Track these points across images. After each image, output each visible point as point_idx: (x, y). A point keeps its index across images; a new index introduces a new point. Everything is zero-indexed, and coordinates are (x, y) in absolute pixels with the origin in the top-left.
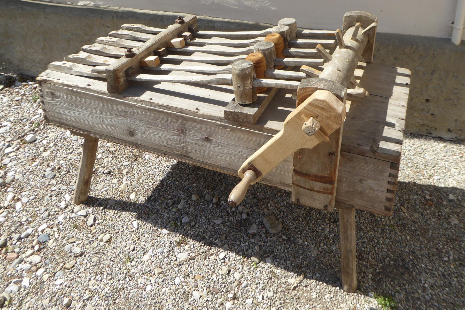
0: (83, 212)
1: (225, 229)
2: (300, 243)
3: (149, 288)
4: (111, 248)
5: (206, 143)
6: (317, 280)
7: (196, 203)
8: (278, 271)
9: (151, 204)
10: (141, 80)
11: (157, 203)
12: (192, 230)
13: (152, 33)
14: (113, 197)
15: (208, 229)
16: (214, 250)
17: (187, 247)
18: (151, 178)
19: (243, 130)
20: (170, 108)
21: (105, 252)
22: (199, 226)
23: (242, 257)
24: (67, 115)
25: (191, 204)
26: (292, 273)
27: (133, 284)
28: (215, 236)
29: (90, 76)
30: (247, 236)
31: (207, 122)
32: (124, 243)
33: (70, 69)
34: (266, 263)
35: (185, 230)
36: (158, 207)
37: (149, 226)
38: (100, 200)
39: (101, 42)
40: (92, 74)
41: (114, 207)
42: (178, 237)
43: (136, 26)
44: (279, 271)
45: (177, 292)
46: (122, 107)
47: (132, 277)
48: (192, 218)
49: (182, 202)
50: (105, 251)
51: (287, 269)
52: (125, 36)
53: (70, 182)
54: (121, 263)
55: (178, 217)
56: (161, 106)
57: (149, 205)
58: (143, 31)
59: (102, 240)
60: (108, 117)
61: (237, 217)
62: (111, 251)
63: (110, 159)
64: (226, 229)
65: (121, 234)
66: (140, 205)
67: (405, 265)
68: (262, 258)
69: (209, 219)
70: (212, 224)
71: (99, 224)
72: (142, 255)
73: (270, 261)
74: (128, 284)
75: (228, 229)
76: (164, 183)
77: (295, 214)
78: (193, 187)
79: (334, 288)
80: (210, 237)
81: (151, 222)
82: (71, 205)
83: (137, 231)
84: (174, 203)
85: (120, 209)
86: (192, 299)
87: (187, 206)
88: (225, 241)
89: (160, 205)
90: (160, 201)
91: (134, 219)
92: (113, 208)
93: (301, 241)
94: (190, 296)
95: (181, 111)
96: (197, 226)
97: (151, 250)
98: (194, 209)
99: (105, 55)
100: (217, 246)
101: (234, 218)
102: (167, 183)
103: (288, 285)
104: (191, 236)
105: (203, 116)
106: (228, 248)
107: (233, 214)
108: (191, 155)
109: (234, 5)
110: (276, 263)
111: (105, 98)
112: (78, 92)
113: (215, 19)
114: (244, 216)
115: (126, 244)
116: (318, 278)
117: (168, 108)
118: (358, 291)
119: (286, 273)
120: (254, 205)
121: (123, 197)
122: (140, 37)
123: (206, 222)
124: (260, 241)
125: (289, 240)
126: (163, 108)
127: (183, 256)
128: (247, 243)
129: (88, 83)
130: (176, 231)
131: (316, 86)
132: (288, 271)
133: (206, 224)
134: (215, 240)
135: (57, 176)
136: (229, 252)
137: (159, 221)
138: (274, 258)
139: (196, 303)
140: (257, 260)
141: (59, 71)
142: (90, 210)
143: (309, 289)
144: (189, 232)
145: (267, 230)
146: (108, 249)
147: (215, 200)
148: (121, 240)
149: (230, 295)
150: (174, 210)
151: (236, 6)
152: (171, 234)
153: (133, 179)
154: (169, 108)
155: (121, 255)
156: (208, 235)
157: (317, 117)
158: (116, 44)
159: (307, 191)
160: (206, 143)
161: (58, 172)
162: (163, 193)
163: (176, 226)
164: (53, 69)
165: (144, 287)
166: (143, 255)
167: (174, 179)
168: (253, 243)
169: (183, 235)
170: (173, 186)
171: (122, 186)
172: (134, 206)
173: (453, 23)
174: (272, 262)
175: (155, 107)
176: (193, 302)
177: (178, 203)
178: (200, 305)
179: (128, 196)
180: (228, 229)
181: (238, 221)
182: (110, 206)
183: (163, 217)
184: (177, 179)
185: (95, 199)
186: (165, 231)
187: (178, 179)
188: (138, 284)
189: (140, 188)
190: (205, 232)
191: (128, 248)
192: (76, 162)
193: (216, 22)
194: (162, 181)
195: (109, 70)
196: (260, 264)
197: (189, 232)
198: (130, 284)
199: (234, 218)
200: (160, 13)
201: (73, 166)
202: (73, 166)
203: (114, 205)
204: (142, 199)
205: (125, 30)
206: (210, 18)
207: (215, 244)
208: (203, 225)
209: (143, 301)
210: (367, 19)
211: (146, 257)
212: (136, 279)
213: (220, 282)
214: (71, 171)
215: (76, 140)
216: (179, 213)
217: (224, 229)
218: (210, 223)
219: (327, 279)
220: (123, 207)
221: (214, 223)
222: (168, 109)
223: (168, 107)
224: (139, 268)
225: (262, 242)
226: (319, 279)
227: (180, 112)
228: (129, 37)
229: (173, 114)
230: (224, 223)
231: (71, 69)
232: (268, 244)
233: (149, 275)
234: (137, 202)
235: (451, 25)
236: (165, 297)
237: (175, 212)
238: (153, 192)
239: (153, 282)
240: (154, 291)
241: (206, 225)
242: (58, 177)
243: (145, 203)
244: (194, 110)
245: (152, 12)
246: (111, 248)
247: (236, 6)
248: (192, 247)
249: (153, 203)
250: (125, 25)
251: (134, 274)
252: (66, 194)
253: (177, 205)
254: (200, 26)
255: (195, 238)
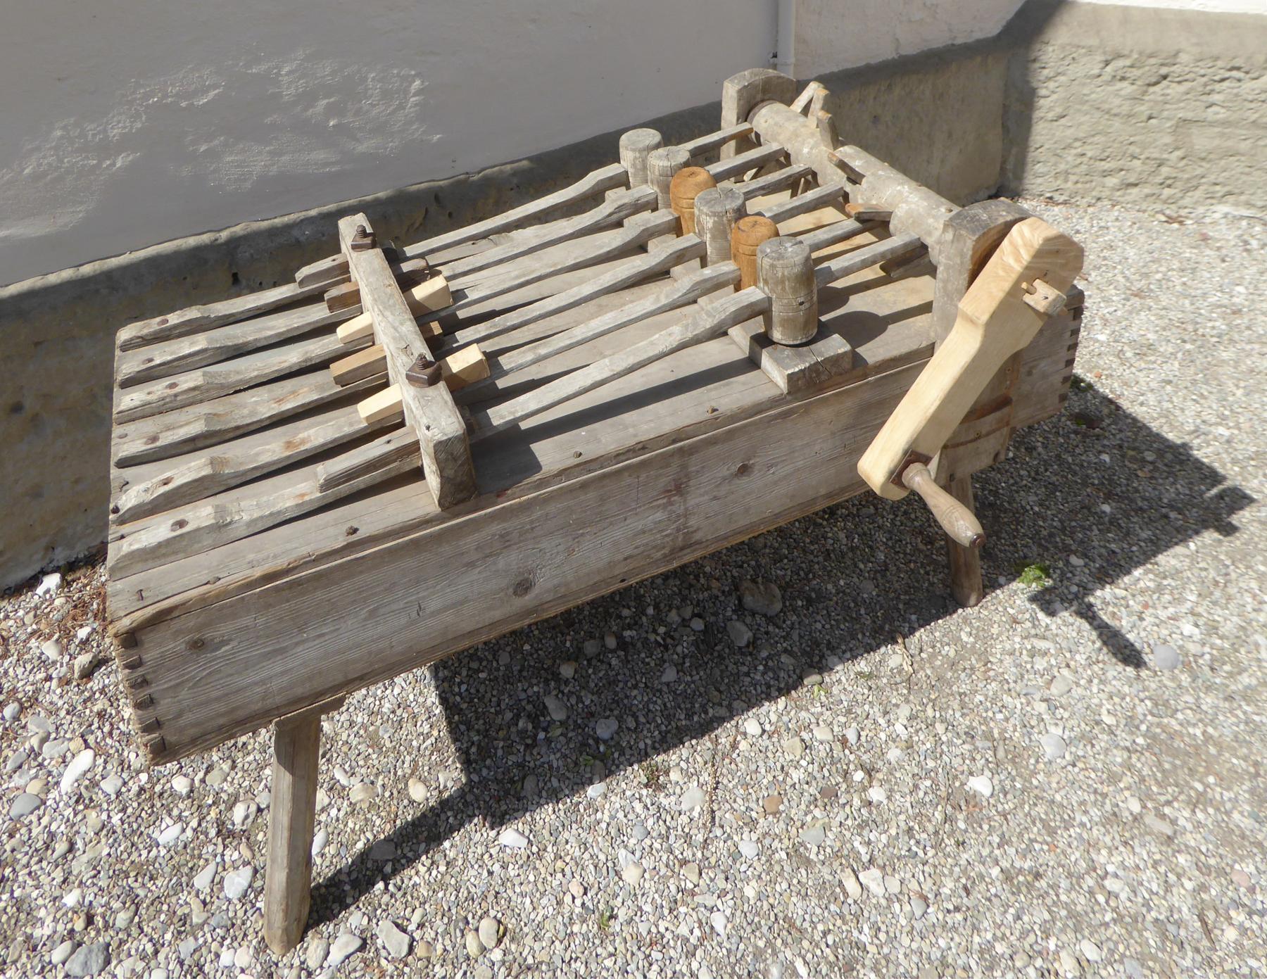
0: (343, 945)
1: (697, 677)
2: (834, 591)
3: (718, 921)
4: (529, 940)
5: (739, 482)
6: (922, 626)
7: (581, 679)
8: (862, 665)
9: (489, 768)
10: (509, 426)
11: (500, 752)
12: (641, 736)
13: (251, 314)
14: (371, 838)
15: (668, 705)
16: (724, 734)
17: (674, 776)
18: (405, 715)
19: (827, 398)
20: (643, 447)
21: (530, 961)
22: (646, 716)
23: (783, 698)
24: (262, 682)
25: (572, 690)
26: (883, 649)
27: (679, 950)
28: (697, 705)
29: (316, 506)
30: (743, 654)
31: (745, 426)
32: (544, 901)
33: (220, 527)
34: (832, 669)
35: (631, 748)
36: (512, 759)
37: (547, 814)
38: (344, 877)
39: (139, 414)
40: (323, 496)
41: (405, 856)
42: (636, 773)
43: (174, 319)
44: (863, 663)
45: (777, 868)
46: (496, 528)
47: (657, 941)
48: (616, 712)
49: (550, 703)
50: (525, 960)
51: (870, 649)
52: (190, 360)
53: (184, 919)
54: (597, 942)
55: (580, 738)
56: (618, 456)
57: (485, 772)
58: (214, 324)
59: (483, 950)
60: (438, 587)
61: (685, 638)
62: (537, 946)
63: (226, 766)
64: (698, 677)
65: (510, 892)
66: (462, 793)
67: (984, 503)
68: (822, 667)
69: (646, 686)
70: (665, 689)
71: (421, 926)
72: (616, 879)
73: (836, 659)
74: (668, 962)
75: (702, 673)
76: (451, 700)
77: (767, 551)
78: (531, 655)
79: (955, 616)
80: (689, 716)
81: (542, 801)
82: (277, 965)
83: (535, 849)
84: (534, 719)
85: (423, 846)
86: (815, 849)
87: (573, 700)
88: (723, 697)
89: (508, 749)
90: (501, 744)
91: (493, 834)
92: (403, 861)
93: (830, 586)
94: (802, 849)
95: (677, 436)
96: (642, 720)
97: (622, 853)
98: (593, 694)
99: (231, 435)
100: (722, 720)
101: (685, 644)
102: (460, 694)
103: (900, 672)
104: (654, 748)
105: (733, 418)
106: (745, 705)
107: (673, 638)
108: (697, 536)
109: (326, 164)
110: (848, 655)
111: (431, 536)
112: (318, 576)
113: (278, 221)
114: (698, 625)
115: (553, 898)
116: (921, 622)
117: (639, 450)
118: (987, 590)
119: (876, 656)
120: (685, 592)
121: (396, 816)
122: (250, 339)
123: (651, 696)
124: (777, 643)
125: (810, 602)
126: (624, 458)
127: (692, 799)
128: (761, 668)
129: (345, 527)
130: (613, 768)
131: (1001, 221)
132: (874, 651)
133: (654, 699)
134: (706, 713)
135: (114, 944)
136: (754, 710)
137: (555, 782)
138: (832, 649)
139: (828, 850)
140: (815, 678)
141: (173, 558)
142: (355, 918)
143: (931, 650)
144: (642, 745)
145: (765, 616)
146: (527, 950)
147: (611, 642)
148: (528, 901)
149: (859, 776)
150: (559, 732)
151: (333, 164)
152: (614, 783)
153: (362, 756)
154: (644, 448)
155: (576, 929)
156: (682, 717)
157: (1046, 275)
158: (208, 391)
159: (970, 445)
160: (744, 481)
161: (98, 932)
162: (481, 722)
163: (603, 758)
164: (139, 566)
165: (707, 929)
166: (620, 878)
167: (464, 673)
168: (770, 657)
169: (640, 762)
170: (482, 690)
171: (357, 793)
172: (451, 809)
173: (775, 56)
174: (842, 660)
175: (602, 468)
176: (822, 852)
177: (544, 710)
178: (838, 844)
179: (406, 802)
180: (702, 673)
181: (695, 644)
182: (390, 864)
183: (551, 767)
184: (470, 669)
185: (326, 887)
186: (594, 791)
187: (474, 665)
188: (688, 940)
189: (408, 758)
190: (669, 718)
191: (568, 899)
192: (125, 856)
193: (288, 227)
194: (444, 700)
195: (450, 439)
196: (827, 679)
197: (642, 745)
198: (671, 959)
199: (685, 644)
200: (87, 269)
201: (132, 874)
202: (132, 874)
203: (399, 852)
204: (451, 777)
205: (139, 346)
206: (265, 224)
207: (712, 721)
208: (651, 706)
209: (743, 955)
210: (780, 80)
211: (631, 875)
212: (668, 935)
213: (815, 773)
214: (141, 893)
215: (38, 808)
216: (573, 730)
217: (695, 678)
218: (660, 691)
219: (934, 611)
220: (425, 834)
221: (668, 684)
222: (640, 452)
223: (640, 446)
224: (648, 908)
225: (782, 640)
226: (924, 622)
227: (674, 442)
228: (209, 357)
229: (657, 455)
230: (680, 667)
231: (230, 523)
232: (795, 637)
233: (689, 900)
234: (446, 795)
235: (772, 60)
236: (771, 900)
237: (562, 734)
238: (455, 740)
239: (710, 900)
240: (738, 913)
241: (655, 703)
242: (122, 942)
243: (470, 781)
244: (708, 416)
245: (53, 279)
246: (529, 940)
247: (333, 164)
248: (683, 764)
249: (488, 762)
250: (124, 334)
251: (654, 930)
252: (218, 956)
253: (548, 718)
254: (252, 255)
255: (668, 742)
